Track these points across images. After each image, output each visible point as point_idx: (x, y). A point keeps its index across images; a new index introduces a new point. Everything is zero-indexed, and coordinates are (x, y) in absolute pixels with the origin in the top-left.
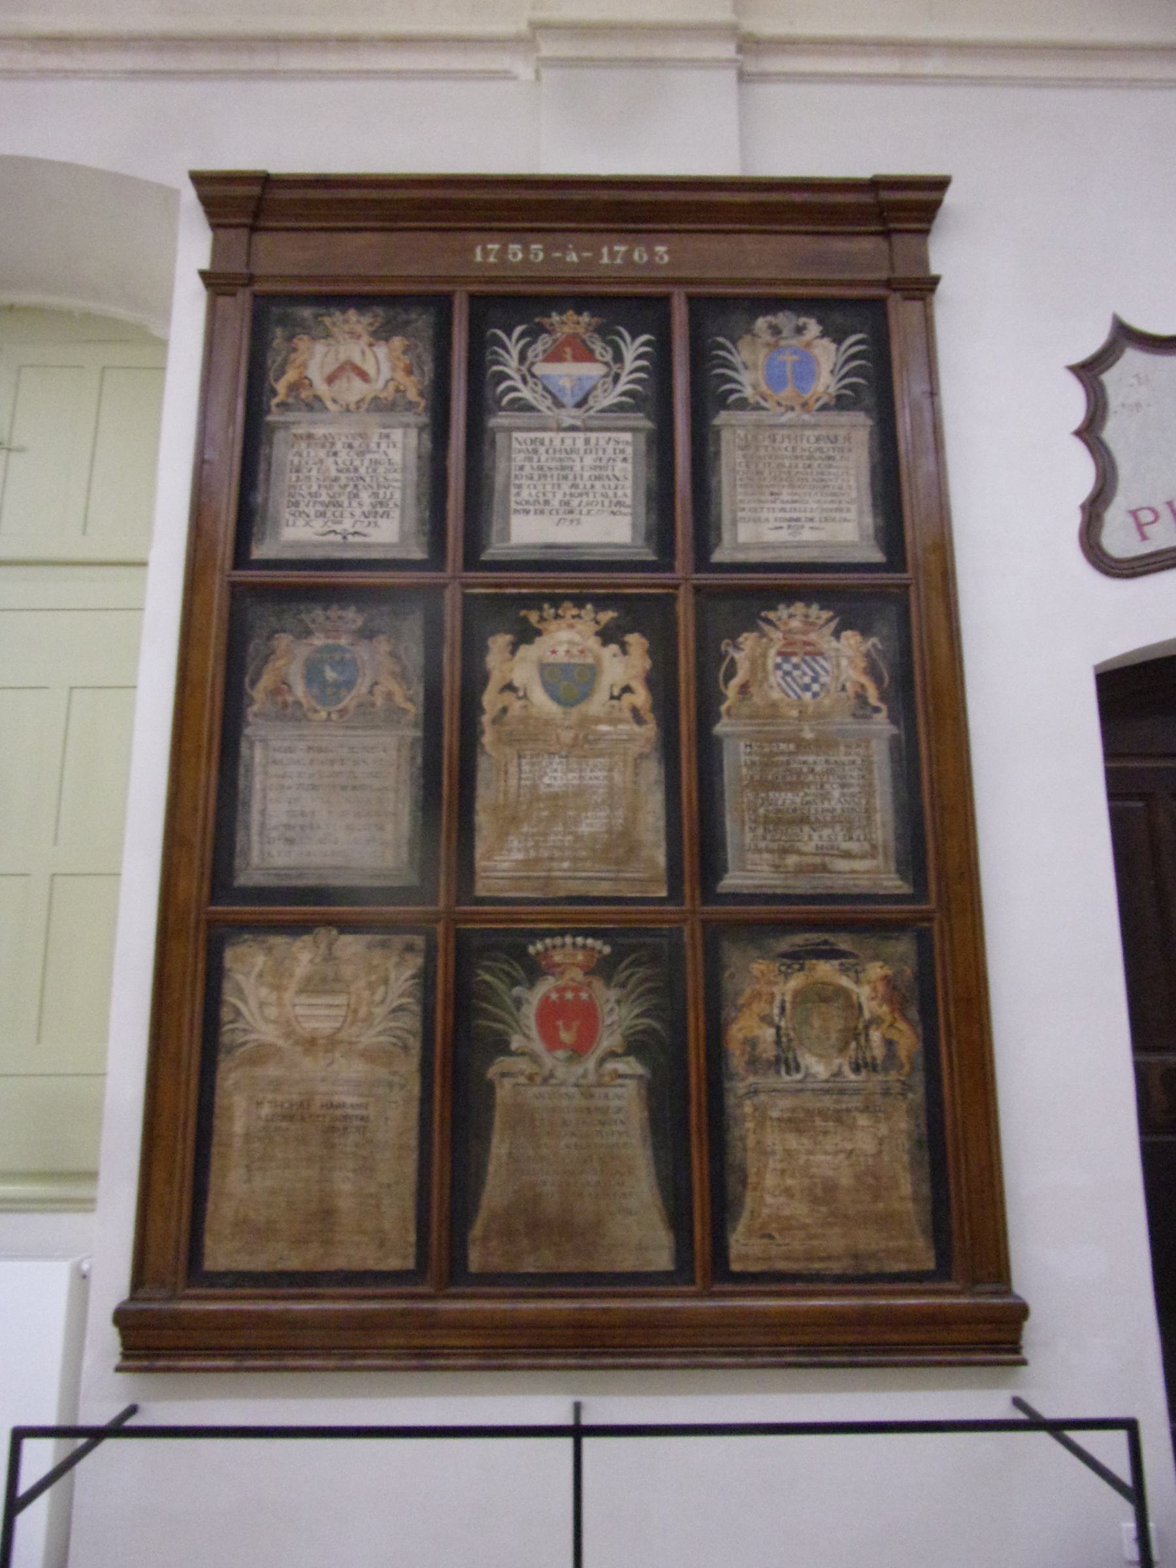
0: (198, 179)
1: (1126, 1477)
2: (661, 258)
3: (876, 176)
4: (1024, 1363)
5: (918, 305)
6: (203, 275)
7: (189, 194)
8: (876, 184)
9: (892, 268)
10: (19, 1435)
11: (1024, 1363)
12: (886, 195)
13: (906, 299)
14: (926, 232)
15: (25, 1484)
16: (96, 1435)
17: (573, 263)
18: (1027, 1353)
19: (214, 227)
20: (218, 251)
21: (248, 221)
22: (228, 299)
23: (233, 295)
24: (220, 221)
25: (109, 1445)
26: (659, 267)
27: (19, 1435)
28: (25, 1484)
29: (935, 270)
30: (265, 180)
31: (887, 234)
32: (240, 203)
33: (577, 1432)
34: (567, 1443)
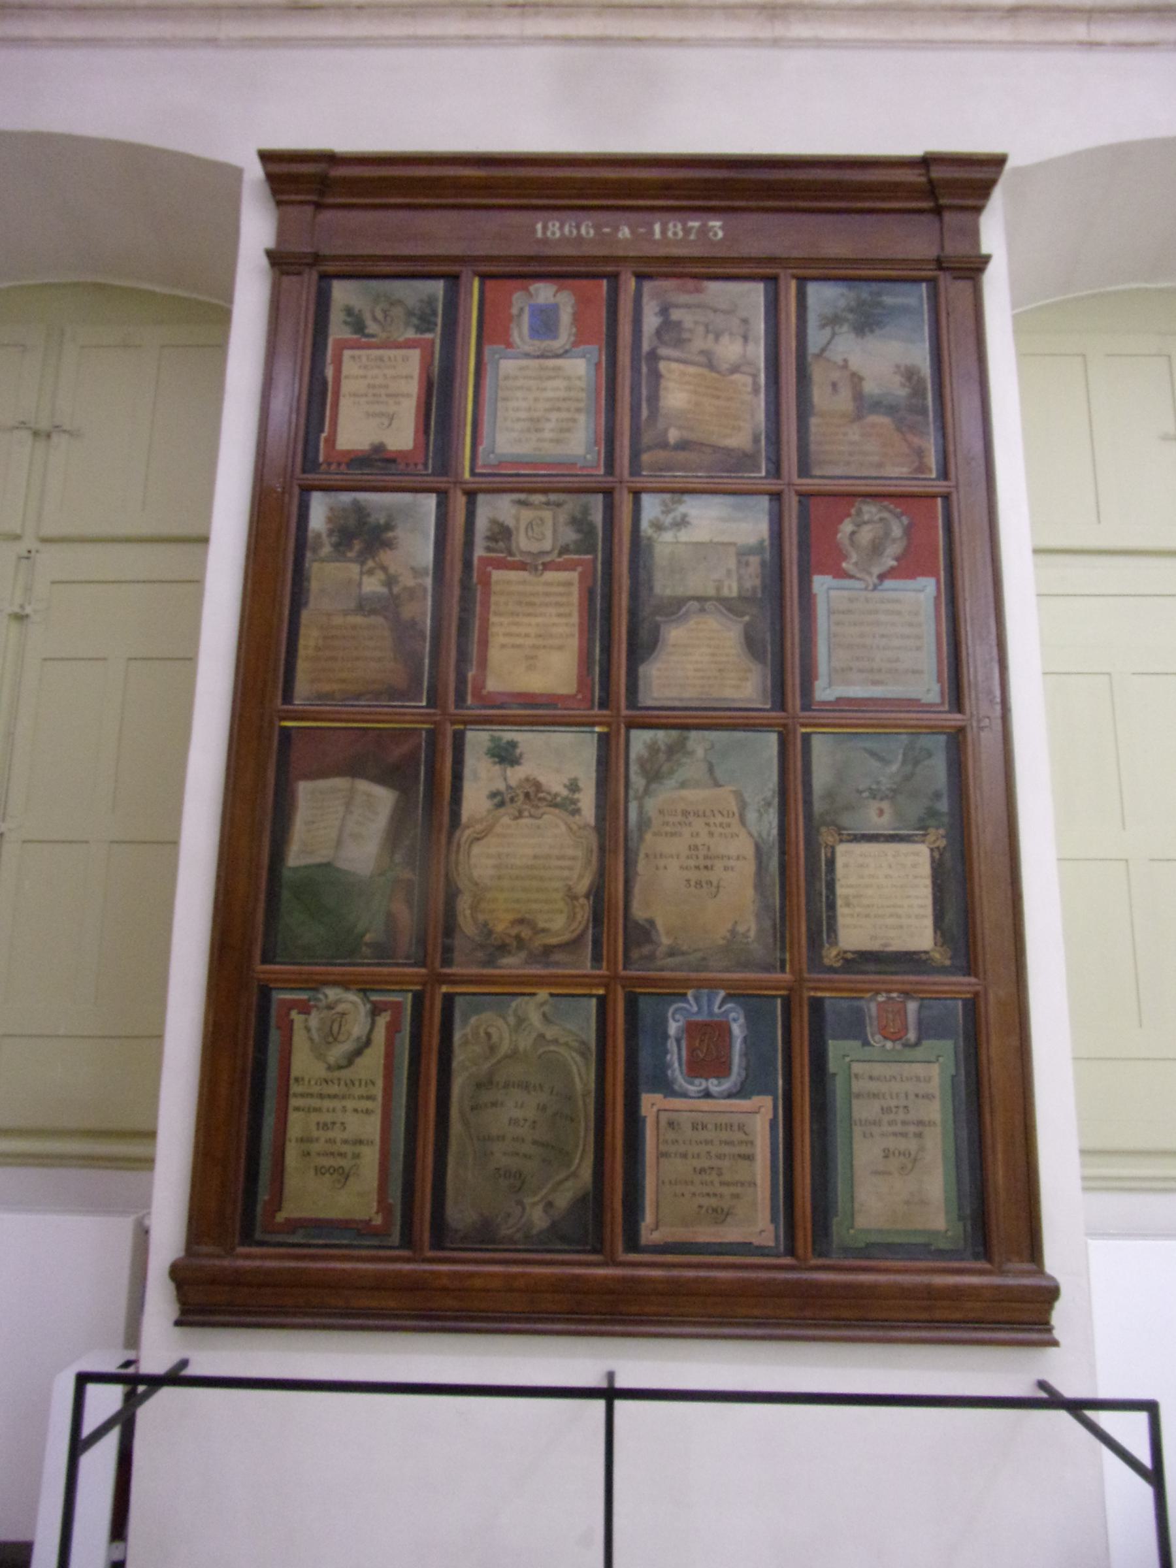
0: (267, 157)
1: (1146, 1459)
2: (716, 234)
3: (926, 153)
4: (1055, 1343)
5: (964, 286)
6: (270, 254)
7: (255, 172)
8: (927, 162)
9: (942, 248)
10: (83, 1379)
11: (1055, 1343)
12: (937, 173)
13: (955, 278)
14: (978, 210)
15: (89, 1427)
16: (156, 1382)
17: (627, 240)
18: (1057, 1334)
19: (279, 203)
20: (282, 232)
21: (314, 198)
22: (294, 278)
23: (299, 274)
24: (285, 198)
25: (166, 1393)
26: (713, 244)
27: (1151, 1408)
28: (89, 1427)
29: (985, 250)
30: (331, 158)
31: (938, 211)
32: (298, 179)
33: (610, 1394)
34: (600, 1405)
